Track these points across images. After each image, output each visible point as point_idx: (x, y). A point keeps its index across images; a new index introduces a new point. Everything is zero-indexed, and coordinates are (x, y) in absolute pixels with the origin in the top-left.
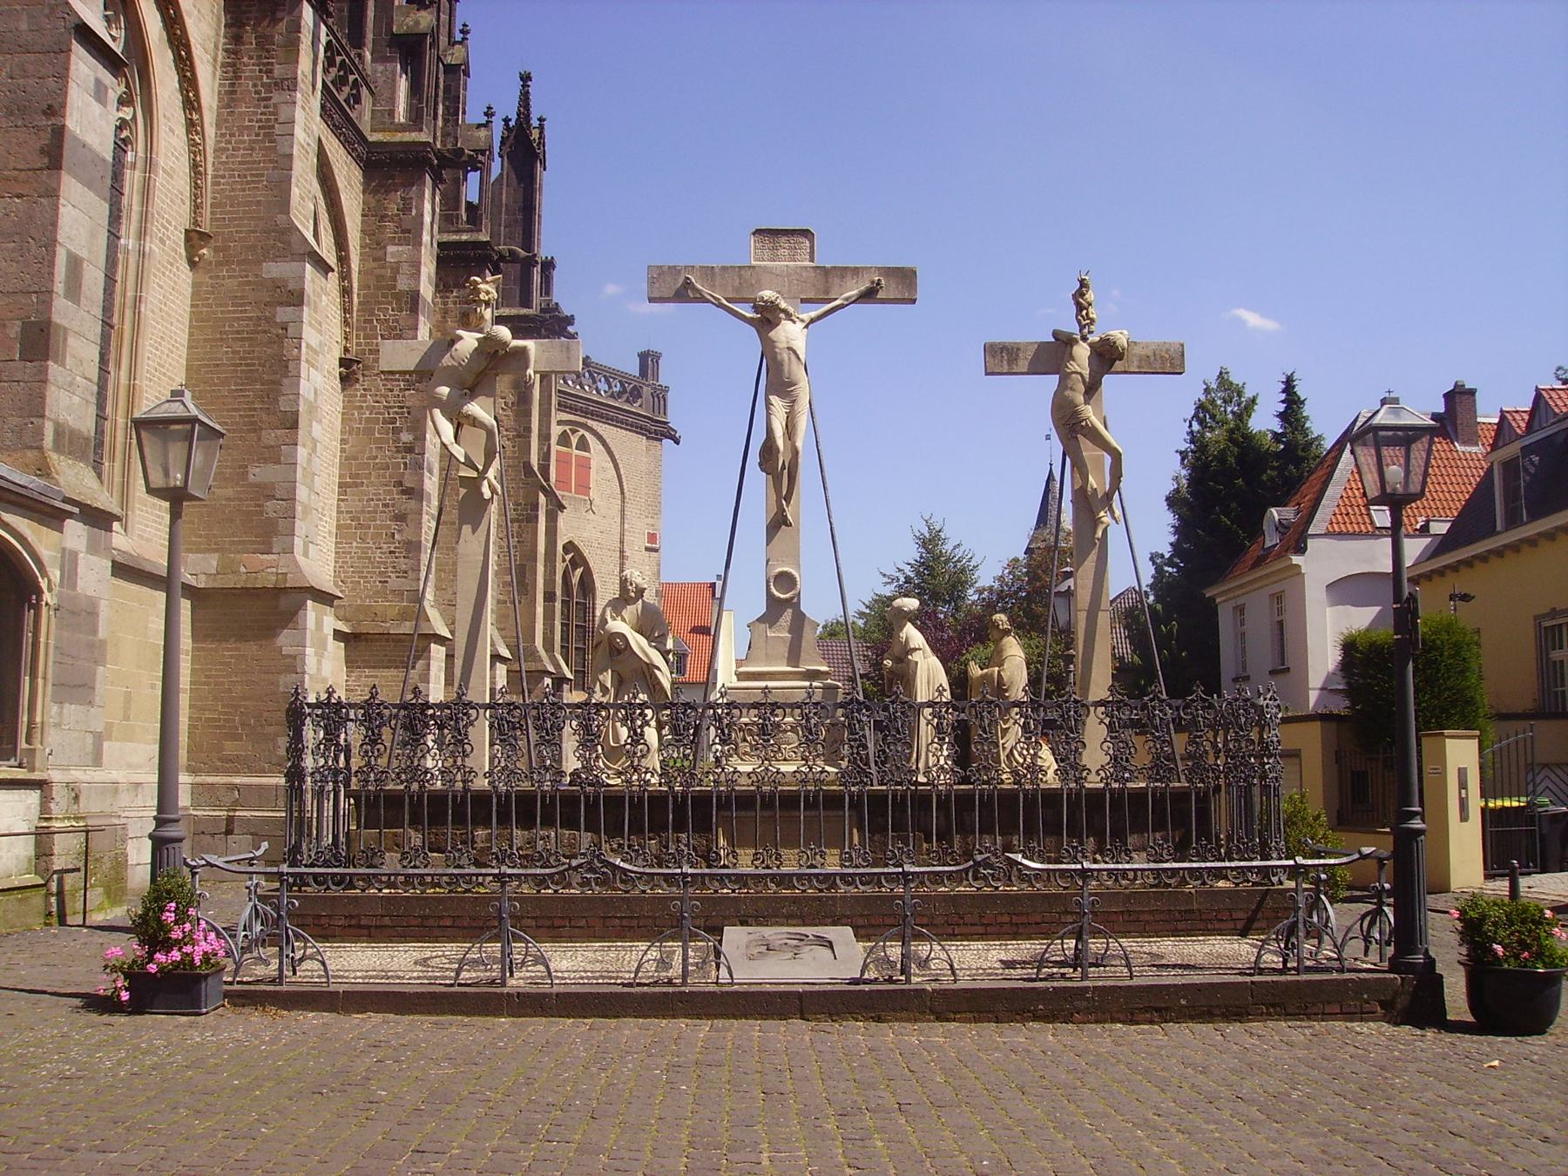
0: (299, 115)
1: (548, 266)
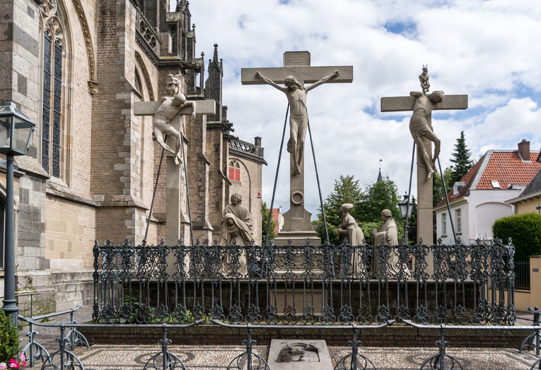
0: (127, 40)
1: (225, 108)
